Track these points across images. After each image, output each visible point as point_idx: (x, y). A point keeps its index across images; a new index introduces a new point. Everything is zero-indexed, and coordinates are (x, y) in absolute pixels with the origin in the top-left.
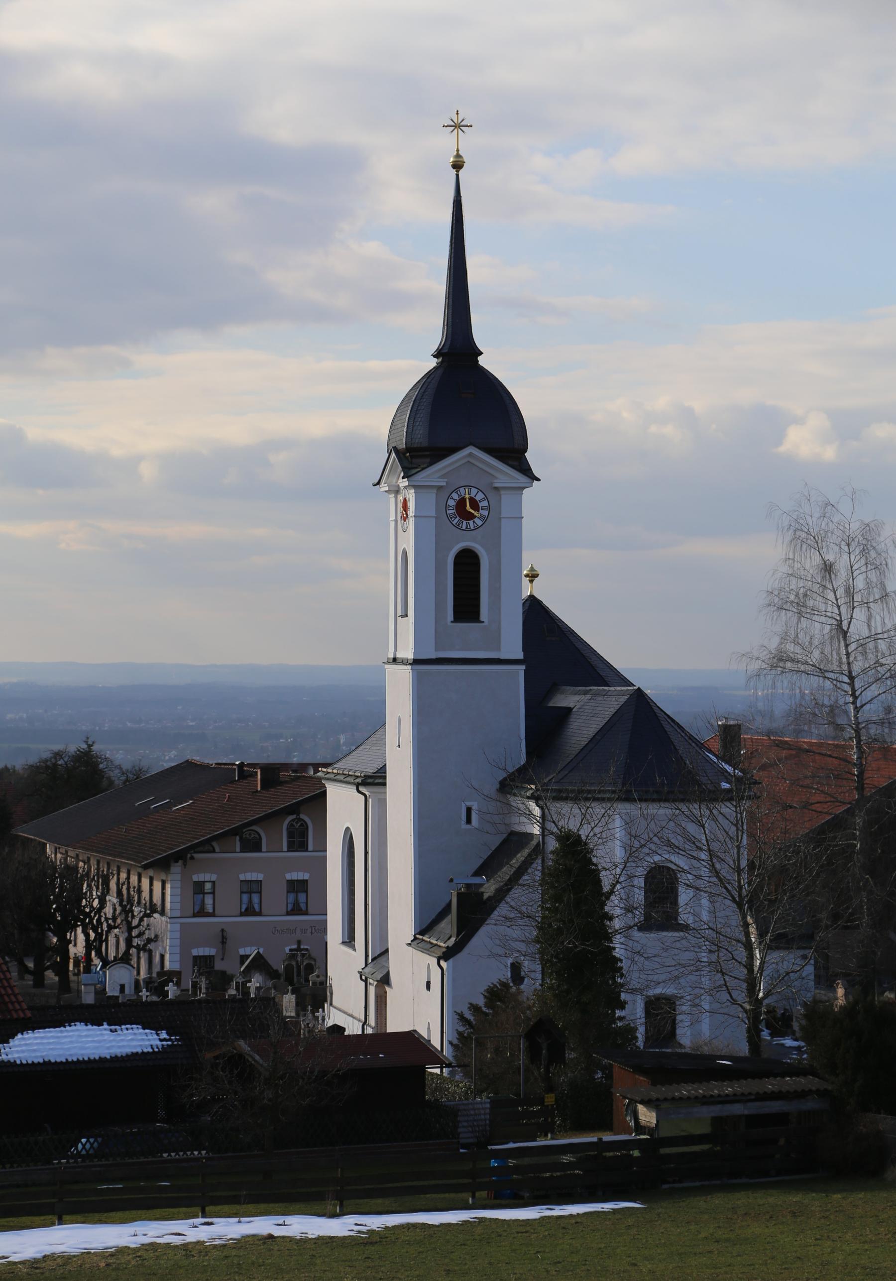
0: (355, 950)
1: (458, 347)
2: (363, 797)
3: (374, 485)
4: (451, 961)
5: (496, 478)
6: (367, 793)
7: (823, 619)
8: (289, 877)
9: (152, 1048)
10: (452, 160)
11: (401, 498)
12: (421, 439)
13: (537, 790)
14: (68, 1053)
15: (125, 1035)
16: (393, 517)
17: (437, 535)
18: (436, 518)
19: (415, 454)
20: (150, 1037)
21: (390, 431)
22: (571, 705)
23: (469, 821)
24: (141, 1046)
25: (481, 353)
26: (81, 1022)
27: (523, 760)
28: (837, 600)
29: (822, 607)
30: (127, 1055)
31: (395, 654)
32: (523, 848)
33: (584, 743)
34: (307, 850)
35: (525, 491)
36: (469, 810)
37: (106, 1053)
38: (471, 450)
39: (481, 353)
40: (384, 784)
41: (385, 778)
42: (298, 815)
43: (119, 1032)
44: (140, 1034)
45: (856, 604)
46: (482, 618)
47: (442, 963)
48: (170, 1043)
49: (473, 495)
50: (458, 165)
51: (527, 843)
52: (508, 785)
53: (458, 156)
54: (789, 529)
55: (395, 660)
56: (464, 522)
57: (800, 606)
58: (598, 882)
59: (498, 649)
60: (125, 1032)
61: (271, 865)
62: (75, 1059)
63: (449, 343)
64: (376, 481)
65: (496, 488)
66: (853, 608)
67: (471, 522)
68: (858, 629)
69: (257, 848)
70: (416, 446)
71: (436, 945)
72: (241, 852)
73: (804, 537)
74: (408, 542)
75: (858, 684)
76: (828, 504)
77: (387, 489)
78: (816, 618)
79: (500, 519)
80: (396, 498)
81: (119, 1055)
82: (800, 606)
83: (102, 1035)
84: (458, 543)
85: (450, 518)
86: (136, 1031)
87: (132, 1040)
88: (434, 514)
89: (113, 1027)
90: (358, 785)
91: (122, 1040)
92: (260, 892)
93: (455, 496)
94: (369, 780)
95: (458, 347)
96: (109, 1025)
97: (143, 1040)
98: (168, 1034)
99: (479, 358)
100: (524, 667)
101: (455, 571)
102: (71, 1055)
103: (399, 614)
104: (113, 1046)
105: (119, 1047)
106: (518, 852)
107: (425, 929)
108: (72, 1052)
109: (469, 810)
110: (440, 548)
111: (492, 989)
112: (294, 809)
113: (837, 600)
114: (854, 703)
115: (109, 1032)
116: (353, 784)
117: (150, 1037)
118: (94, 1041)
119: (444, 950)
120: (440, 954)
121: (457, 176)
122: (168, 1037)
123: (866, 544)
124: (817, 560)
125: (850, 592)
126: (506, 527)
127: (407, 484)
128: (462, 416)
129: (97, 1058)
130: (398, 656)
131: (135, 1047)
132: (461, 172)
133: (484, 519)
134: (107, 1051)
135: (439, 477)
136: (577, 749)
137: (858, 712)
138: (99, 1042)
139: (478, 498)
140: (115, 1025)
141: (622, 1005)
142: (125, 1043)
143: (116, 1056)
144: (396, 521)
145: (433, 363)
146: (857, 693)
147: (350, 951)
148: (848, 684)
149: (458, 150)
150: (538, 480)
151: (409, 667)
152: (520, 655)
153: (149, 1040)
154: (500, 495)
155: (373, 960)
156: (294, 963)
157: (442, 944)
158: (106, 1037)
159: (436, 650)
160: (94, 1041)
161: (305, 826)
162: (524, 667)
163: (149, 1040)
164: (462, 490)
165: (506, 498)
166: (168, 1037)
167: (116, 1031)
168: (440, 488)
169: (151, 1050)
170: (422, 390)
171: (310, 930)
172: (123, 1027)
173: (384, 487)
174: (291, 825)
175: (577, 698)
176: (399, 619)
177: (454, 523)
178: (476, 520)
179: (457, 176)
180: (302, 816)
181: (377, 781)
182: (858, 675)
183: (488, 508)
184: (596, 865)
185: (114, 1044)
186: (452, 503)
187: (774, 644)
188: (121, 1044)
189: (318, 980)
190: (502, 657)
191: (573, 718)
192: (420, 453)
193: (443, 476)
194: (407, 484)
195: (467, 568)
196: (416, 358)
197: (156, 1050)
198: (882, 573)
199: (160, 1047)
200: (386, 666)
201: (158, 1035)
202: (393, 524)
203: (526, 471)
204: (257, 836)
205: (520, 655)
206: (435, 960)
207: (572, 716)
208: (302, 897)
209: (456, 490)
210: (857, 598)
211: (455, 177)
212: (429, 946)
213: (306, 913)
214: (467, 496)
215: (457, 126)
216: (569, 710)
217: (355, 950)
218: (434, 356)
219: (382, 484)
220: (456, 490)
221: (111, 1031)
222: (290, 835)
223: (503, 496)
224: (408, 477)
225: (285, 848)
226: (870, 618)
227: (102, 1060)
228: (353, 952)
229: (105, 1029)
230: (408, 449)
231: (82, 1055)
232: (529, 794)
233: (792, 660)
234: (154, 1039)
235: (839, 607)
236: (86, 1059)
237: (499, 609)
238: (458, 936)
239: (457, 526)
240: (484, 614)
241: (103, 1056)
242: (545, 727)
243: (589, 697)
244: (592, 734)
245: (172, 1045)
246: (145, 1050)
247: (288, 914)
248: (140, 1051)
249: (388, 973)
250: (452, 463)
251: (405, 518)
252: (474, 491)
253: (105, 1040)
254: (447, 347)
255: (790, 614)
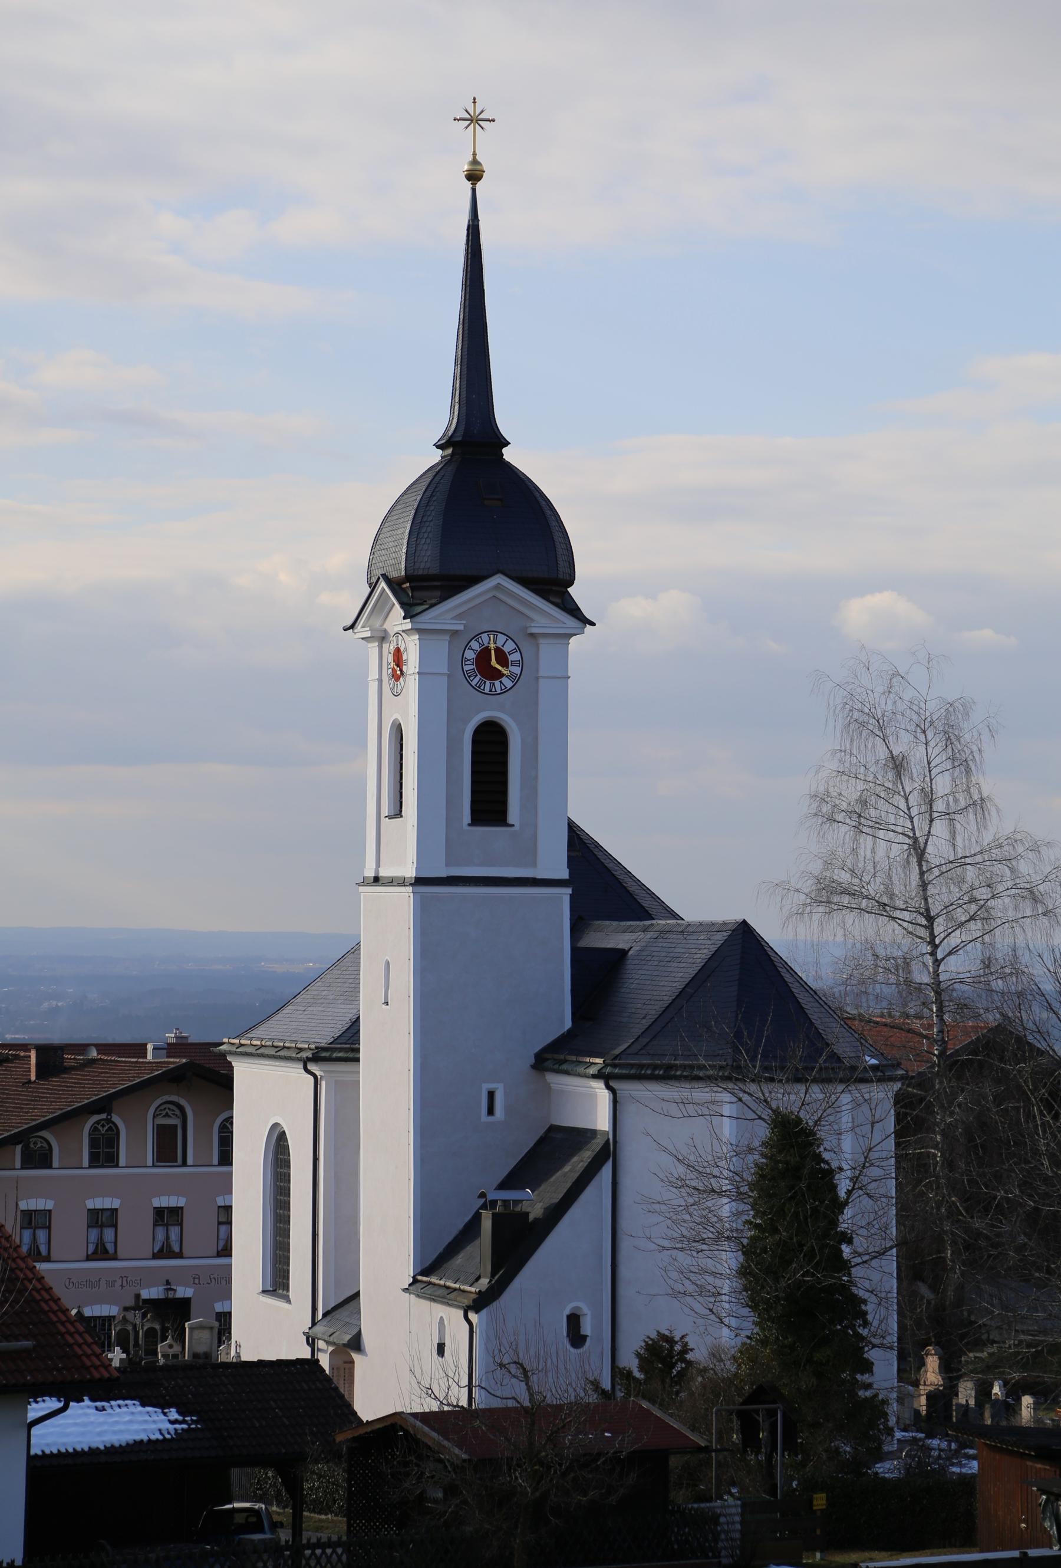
0: (289, 1301)
1: (475, 441)
2: (311, 1078)
3: (346, 630)
4: (484, 1312)
5: (532, 620)
6: (318, 1073)
7: (891, 835)
8: (90, 1204)
9: (161, 1434)
10: (466, 168)
11: (389, 648)
12: (429, 563)
13: (606, 1065)
14: (44, 1442)
15: (118, 1414)
16: (374, 674)
17: (449, 700)
18: (449, 676)
19: (418, 587)
20: (155, 1418)
21: (372, 552)
22: (626, 947)
23: (491, 1111)
24: (145, 1430)
25: (507, 444)
26: (51, 1396)
27: (568, 1024)
28: (909, 809)
29: (892, 819)
30: (128, 1444)
31: (377, 871)
32: (580, 1149)
33: (667, 1000)
34: (117, 1166)
35: (573, 640)
36: (491, 1095)
37: (99, 1441)
38: (499, 579)
39: (507, 444)
40: (358, 1060)
41: (358, 1050)
42: (109, 1114)
43: (109, 1411)
44: (140, 1413)
45: (935, 815)
46: (510, 821)
47: (473, 1317)
48: (185, 1426)
49: (499, 644)
50: (474, 176)
51: (587, 1143)
52: (555, 1057)
53: (475, 162)
54: (844, 708)
55: (376, 880)
56: (488, 682)
57: (860, 818)
58: (834, 1188)
59: (534, 864)
60: (118, 1410)
61: (134, 1184)
62: (55, 1451)
63: (462, 428)
64: (349, 623)
65: (532, 635)
66: (931, 821)
67: (497, 683)
68: (937, 850)
69: (44, 1160)
70: (420, 572)
71: (455, 1290)
72: (22, 1168)
73: (866, 722)
74: (406, 707)
75: (939, 927)
76: (897, 673)
77: (368, 634)
78: (881, 834)
79: (537, 678)
80: (381, 648)
81: (117, 1445)
82: (860, 818)
83: (86, 1415)
84: (478, 713)
85: (467, 676)
86: (132, 1409)
87: (130, 1422)
88: (446, 671)
89: (99, 1404)
90: (305, 1062)
91: (117, 1422)
92: (49, 1228)
93: (475, 645)
94: (324, 1054)
95: (475, 441)
96: (93, 1400)
97: (146, 1422)
98: (179, 1413)
99: (505, 450)
100: (569, 891)
101: (473, 753)
102: (48, 1445)
103: (385, 811)
104: (105, 1432)
105: (115, 1432)
106: (572, 1155)
107: (431, 1270)
108: (49, 1440)
109: (491, 1095)
110: (453, 718)
111: (670, 1340)
112: (104, 1106)
113: (909, 809)
114: (933, 954)
115: (94, 1411)
116: (299, 1059)
117: (155, 1418)
118: (76, 1424)
119: (475, 1296)
120: (467, 1301)
121: (474, 191)
122: (180, 1418)
123: (949, 732)
124: (882, 753)
125: (929, 798)
126: (545, 687)
127: (409, 626)
128: (480, 531)
129: (86, 1449)
130: (383, 873)
131: (137, 1432)
132: (479, 186)
133: (516, 679)
134: (98, 1439)
135: (452, 618)
136: (654, 1010)
137: (939, 966)
138: (84, 1425)
139: (506, 649)
140: (101, 1401)
141: (867, 1367)
142: (122, 1427)
143: (112, 1446)
144: (380, 681)
145: (436, 456)
146: (937, 941)
147: (281, 1304)
148: (925, 926)
149: (474, 154)
150: (593, 624)
151: (410, 889)
152: (564, 874)
153: (154, 1422)
154: (537, 646)
155: (325, 1315)
156: (130, 1328)
157: (467, 1288)
158: (92, 1419)
159: (447, 865)
160: (76, 1424)
161: (115, 1131)
162: (569, 891)
163: (154, 1422)
164: (484, 636)
165: (546, 648)
166: (180, 1418)
167: (103, 1409)
168: (455, 633)
169: (160, 1437)
170: (429, 493)
171: (119, 1282)
172: (113, 1403)
173: (362, 631)
174: (94, 1129)
175: (634, 936)
176: (385, 822)
177: (474, 683)
178: (504, 680)
179: (474, 191)
180: (116, 1118)
181: (335, 1055)
182: (938, 915)
183: (521, 663)
184: (827, 1163)
185: (105, 1428)
186: (470, 655)
187: (816, 867)
188: (116, 1428)
189: (171, 1352)
190: (539, 877)
191: (630, 963)
192: (425, 584)
193: (459, 617)
194: (409, 626)
195: (490, 747)
196: (416, 449)
197: (168, 1436)
198: (968, 772)
199: (173, 1432)
200: (361, 889)
201: (165, 1414)
202: (373, 687)
203: (573, 611)
204: (45, 1145)
205: (564, 874)
206: (461, 1313)
207: (629, 962)
208: (109, 1234)
209: (476, 637)
210: (939, 806)
211: (470, 192)
212: (444, 1292)
213: (114, 1258)
214: (492, 646)
215: (474, 120)
216: (623, 954)
217: (289, 1301)
218: (438, 447)
219: (359, 627)
220: (476, 637)
221: (97, 1408)
222: (94, 1143)
223: (541, 646)
224: (411, 617)
225: (86, 1162)
226: (953, 834)
227: (93, 1452)
228: (285, 1305)
229: (88, 1407)
230: (408, 578)
231: (64, 1444)
232: (592, 1070)
233: (845, 892)
234: (162, 1421)
235: (911, 818)
236: (71, 1450)
237: (536, 808)
238: (493, 1275)
239: (478, 689)
240: (514, 813)
241: (94, 1446)
242: (597, 978)
243: (649, 935)
244: (679, 986)
245: (189, 1430)
246: (153, 1437)
247: (89, 1258)
248: (145, 1438)
249: (359, 1335)
250: (465, 602)
251: (398, 674)
252: (501, 639)
253: (92, 1423)
254: (461, 432)
255: (844, 828)
